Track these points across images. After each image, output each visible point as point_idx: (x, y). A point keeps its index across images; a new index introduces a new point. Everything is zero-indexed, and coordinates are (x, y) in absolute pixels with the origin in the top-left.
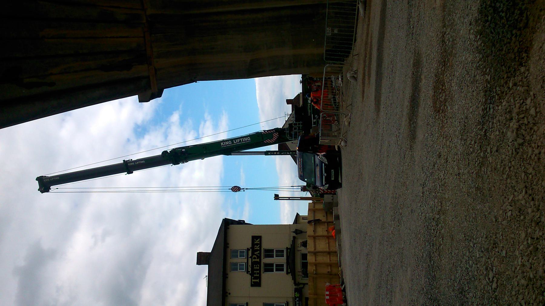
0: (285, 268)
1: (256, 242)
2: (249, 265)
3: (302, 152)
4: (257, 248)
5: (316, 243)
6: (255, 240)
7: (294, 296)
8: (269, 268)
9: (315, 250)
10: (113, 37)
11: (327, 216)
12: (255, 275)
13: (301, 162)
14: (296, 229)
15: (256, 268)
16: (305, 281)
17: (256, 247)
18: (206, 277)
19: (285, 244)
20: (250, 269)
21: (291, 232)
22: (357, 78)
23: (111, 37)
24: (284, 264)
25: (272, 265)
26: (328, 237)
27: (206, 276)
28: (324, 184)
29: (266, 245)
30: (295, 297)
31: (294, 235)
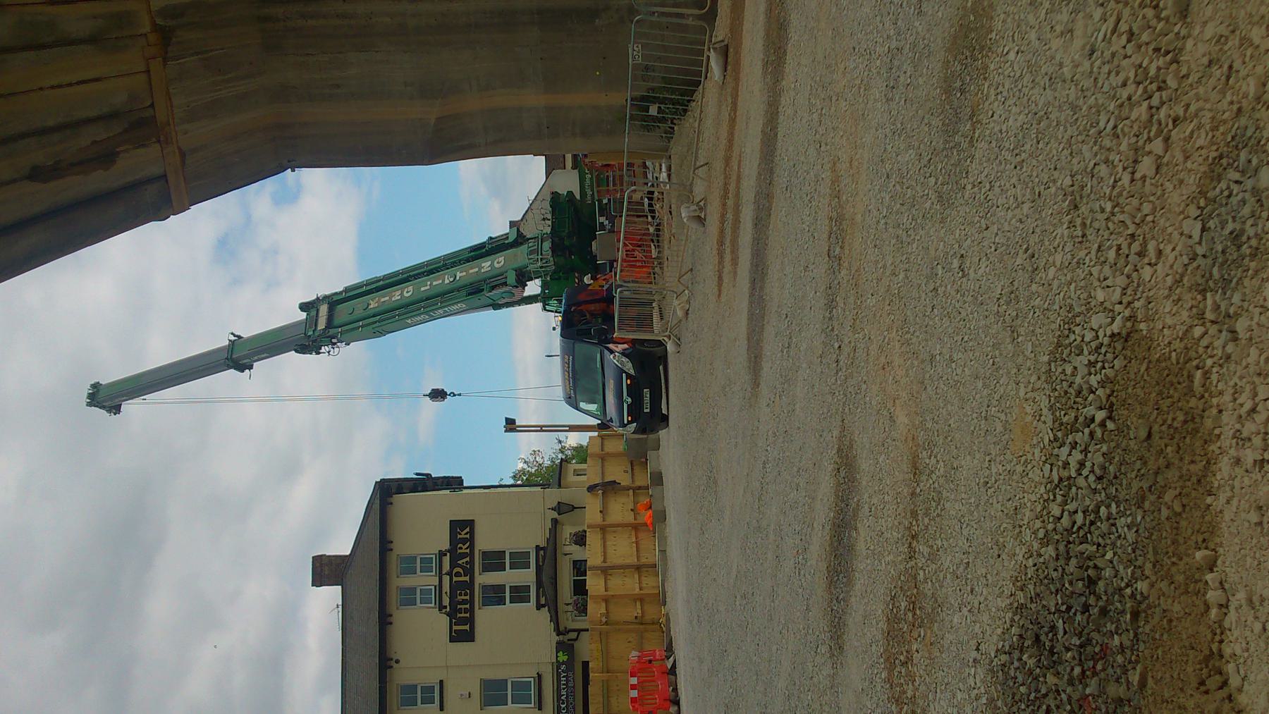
2: (444, 592)
3: (573, 341)
4: (464, 549)
5: (608, 543)
7: (555, 661)
8: (495, 596)
9: (604, 561)
10: (60, 86)
11: (632, 469)
12: (459, 615)
13: (569, 364)
15: (463, 597)
17: (461, 548)
19: (530, 536)
20: (446, 601)
21: (546, 508)
22: (705, 220)
23: (52, 87)
26: (636, 528)
28: (626, 422)
29: (485, 541)
30: (557, 661)
31: (555, 515)
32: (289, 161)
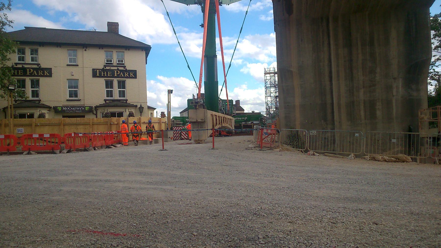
0: (35, 99)
1: (46, 72)
4: (126, 75)
6: (133, 73)
8: (109, 84)
12: (102, 72)
14: (143, 108)
15: (109, 74)
16: (99, 115)
18: (95, 30)
19: (131, 97)
20: (107, 68)
24: (77, 97)
25: (112, 87)
27: (96, 30)
29: (129, 82)
31: (139, 106)
32: (278, 24)
